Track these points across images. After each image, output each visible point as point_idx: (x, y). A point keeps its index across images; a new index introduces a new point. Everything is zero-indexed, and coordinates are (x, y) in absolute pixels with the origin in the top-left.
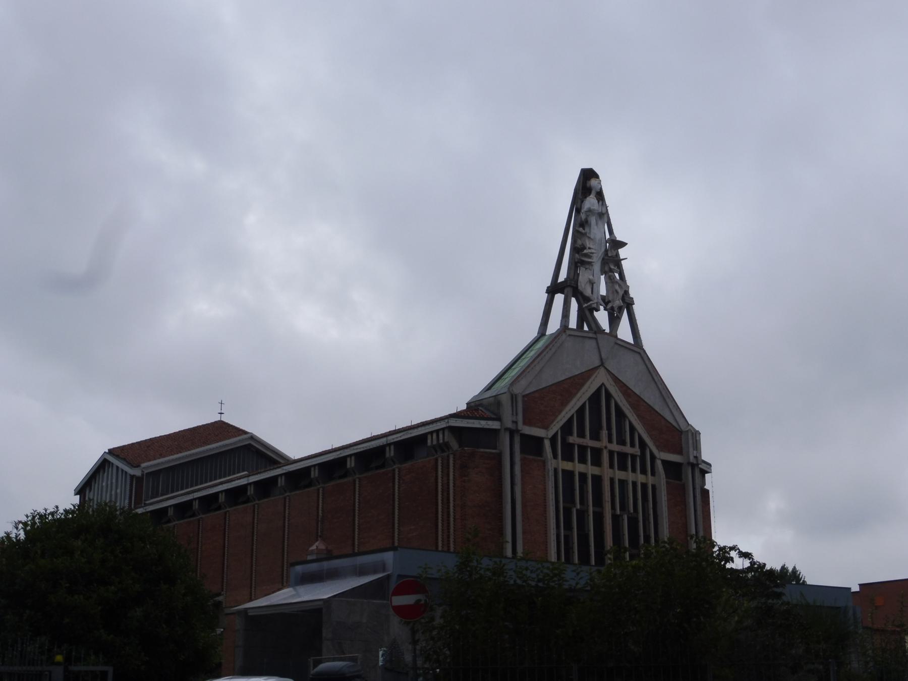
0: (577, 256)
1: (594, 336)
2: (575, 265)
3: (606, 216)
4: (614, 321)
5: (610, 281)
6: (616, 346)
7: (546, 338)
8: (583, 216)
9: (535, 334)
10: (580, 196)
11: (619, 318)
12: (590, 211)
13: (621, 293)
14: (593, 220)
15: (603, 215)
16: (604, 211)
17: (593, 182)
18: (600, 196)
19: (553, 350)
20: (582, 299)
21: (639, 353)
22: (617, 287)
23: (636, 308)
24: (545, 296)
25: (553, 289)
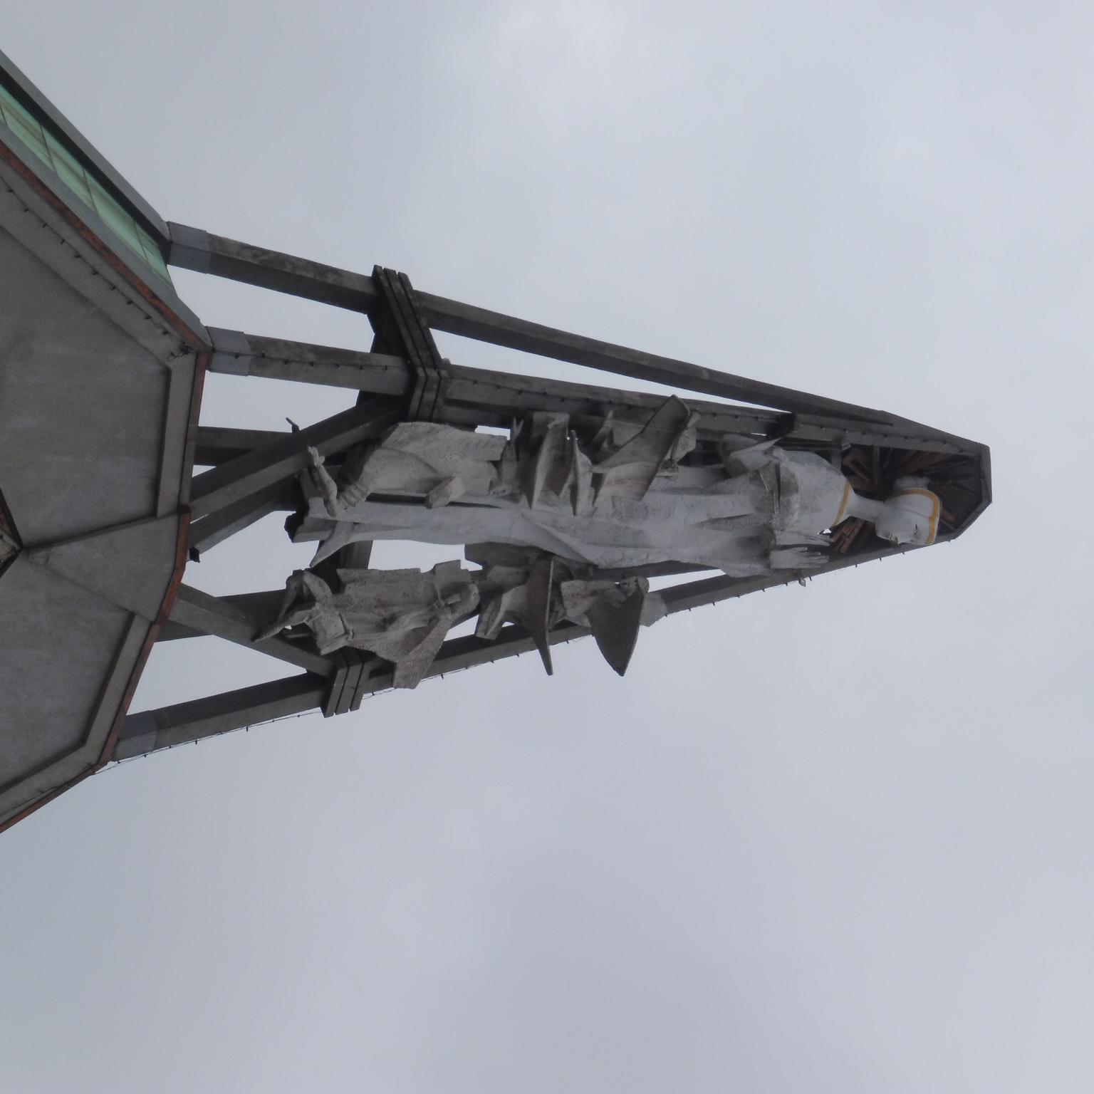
0: (562, 419)
1: (167, 500)
2: (517, 405)
3: (757, 568)
4: (254, 618)
5: (443, 592)
6: (114, 621)
7: (154, 260)
8: (754, 454)
9: (172, 205)
10: (853, 438)
11: (254, 638)
12: (781, 488)
13: (382, 645)
14: (735, 502)
15: (762, 559)
16: (782, 559)
17: (920, 506)
18: (857, 542)
19: (91, 287)
20: (343, 450)
21: (82, 740)
22: (408, 623)
23: (307, 724)
24: (358, 263)
25: (385, 298)
